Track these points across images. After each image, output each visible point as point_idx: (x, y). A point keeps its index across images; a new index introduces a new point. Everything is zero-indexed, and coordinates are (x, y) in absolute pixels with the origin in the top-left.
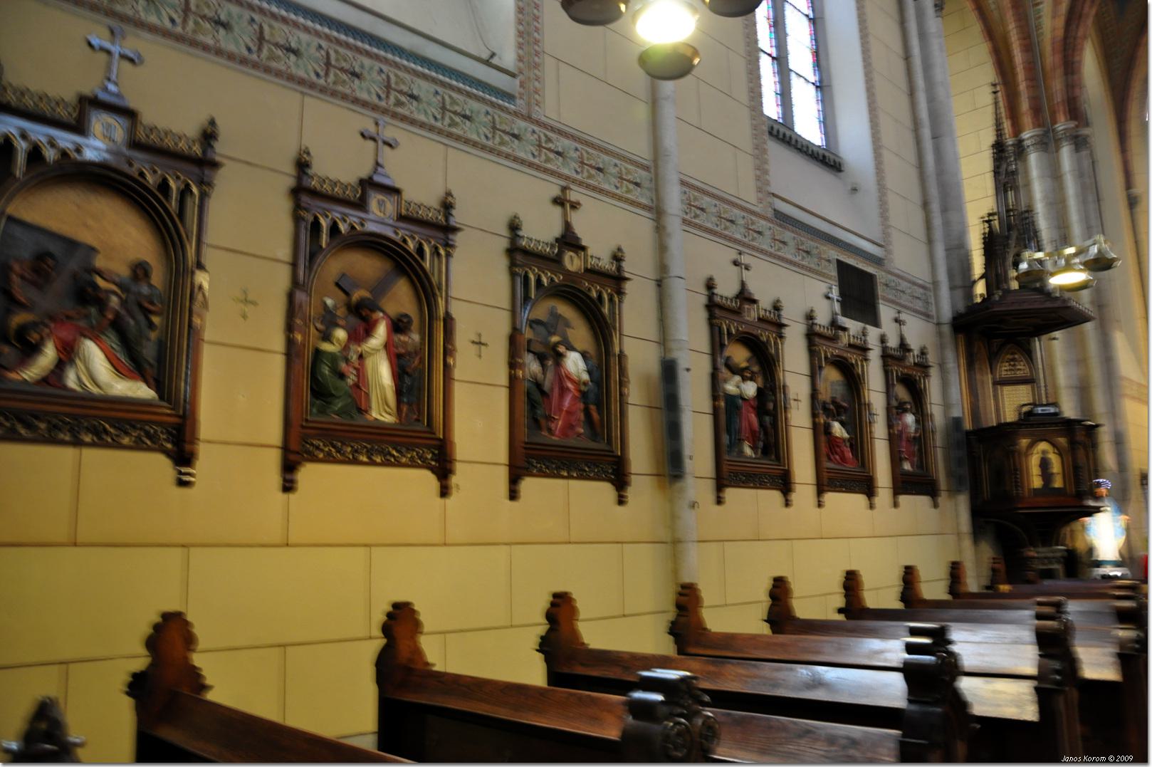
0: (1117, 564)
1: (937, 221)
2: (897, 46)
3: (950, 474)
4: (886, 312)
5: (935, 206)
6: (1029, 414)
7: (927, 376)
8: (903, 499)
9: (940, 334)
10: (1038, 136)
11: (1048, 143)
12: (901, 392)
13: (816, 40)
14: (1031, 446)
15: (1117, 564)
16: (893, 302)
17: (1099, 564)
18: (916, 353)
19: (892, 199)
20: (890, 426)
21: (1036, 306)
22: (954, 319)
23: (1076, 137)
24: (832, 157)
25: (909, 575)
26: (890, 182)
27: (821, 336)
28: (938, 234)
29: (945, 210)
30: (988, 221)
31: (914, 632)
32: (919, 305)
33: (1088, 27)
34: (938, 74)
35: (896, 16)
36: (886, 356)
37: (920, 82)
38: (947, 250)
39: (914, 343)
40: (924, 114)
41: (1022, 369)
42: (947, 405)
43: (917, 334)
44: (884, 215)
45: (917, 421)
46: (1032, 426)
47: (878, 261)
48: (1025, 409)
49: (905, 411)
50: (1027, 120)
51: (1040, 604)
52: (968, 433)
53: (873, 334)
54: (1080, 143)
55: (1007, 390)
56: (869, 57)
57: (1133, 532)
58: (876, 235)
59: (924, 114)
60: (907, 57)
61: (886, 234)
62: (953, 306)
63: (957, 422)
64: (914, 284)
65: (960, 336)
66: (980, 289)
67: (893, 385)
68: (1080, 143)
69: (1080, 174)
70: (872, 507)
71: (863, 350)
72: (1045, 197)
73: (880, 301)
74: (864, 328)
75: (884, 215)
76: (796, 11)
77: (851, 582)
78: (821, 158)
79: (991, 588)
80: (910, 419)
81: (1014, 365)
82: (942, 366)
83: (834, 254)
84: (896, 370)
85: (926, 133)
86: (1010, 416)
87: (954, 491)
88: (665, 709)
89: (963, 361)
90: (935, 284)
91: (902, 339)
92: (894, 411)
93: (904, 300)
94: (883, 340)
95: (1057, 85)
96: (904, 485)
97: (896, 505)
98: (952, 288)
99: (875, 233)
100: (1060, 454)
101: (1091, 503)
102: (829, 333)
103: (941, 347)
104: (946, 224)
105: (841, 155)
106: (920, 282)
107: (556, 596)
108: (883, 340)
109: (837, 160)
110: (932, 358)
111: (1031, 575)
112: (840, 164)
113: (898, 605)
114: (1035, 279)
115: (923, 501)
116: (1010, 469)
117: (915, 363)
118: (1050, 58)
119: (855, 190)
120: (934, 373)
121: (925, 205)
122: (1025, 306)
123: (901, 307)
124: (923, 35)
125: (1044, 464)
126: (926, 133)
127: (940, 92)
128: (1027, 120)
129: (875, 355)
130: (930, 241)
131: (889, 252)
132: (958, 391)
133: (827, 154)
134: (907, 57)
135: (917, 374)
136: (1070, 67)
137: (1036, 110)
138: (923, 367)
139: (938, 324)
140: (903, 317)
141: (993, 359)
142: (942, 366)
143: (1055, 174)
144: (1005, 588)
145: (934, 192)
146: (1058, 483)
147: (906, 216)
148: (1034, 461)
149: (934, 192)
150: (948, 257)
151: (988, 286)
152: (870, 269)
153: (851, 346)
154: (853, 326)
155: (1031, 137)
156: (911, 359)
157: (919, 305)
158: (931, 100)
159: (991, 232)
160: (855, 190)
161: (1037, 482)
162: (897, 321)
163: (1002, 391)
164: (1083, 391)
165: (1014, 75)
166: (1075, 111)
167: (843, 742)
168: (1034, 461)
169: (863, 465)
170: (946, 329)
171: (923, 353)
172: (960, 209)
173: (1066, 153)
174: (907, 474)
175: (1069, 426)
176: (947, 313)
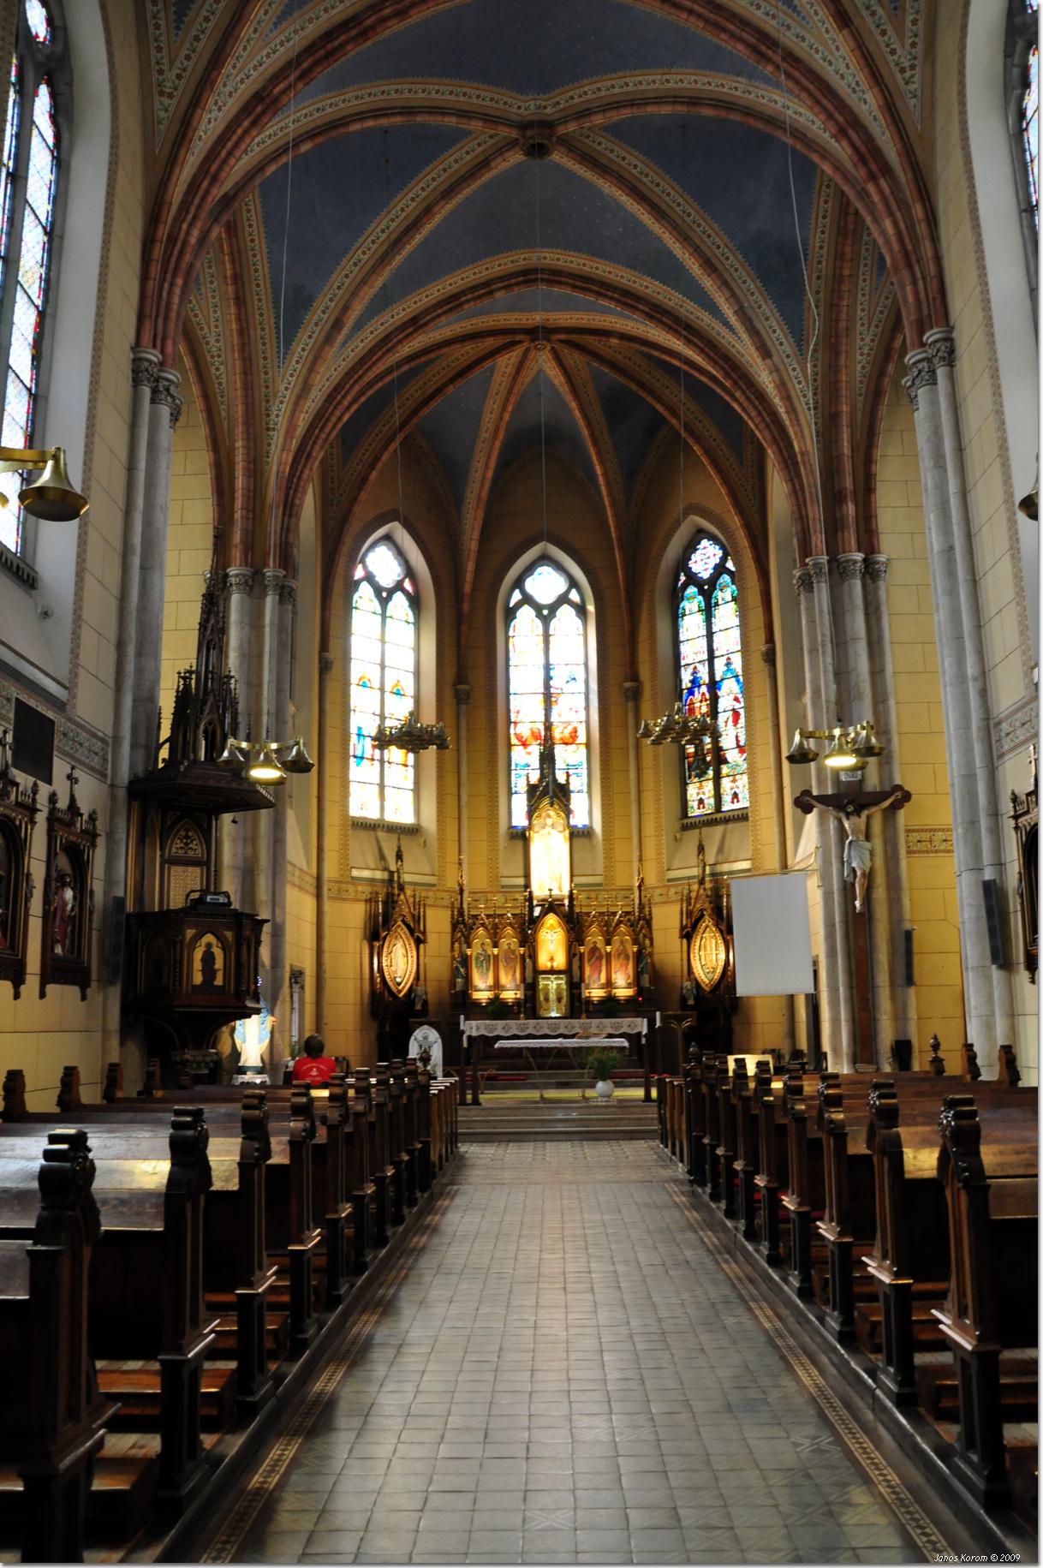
0: (260, 1071)
1: (130, 667)
2: (122, 453)
3: (103, 961)
4: (60, 767)
5: (131, 650)
6: (201, 900)
7: (94, 845)
8: (51, 989)
9: (113, 798)
10: (244, 575)
11: (254, 586)
12: (63, 862)
13: (33, 421)
14: (197, 937)
15: (260, 1071)
16: (67, 754)
17: (242, 1071)
18: (85, 817)
19: (87, 636)
20: (47, 901)
21: (223, 784)
22: (131, 782)
23: (283, 587)
24: (27, 570)
25: (70, 1077)
26: (86, 614)
27: (60, 821)
28: (129, 682)
29: (140, 654)
30: (184, 678)
31: (178, 1113)
32: (96, 762)
33: (313, 470)
34: (160, 496)
35: (127, 416)
36: (52, 819)
37: (140, 502)
38: (134, 701)
39: (85, 807)
40: (137, 540)
41: (196, 849)
42: (109, 881)
43: (89, 794)
44: (75, 652)
45: (75, 898)
46: (199, 915)
47: (60, 706)
48: (196, 896)
49: (64, 885)
50: (236, 554)
51: (178, 1113)
52: (129, 916)
53: (44, 790)
54: (286, 595)
55: (176, 871)
56: (91, 461)
57: (277, 1035)
58: (63, 672)
59: (137, 540)
60: (131, 468)
61: (74, 674)
62: (132, 766)
63: (120, 902)
64: (94, 735)
65: (136, 804)
66: (164, 753)
67: (56, 854)
68: (286, 595)
69: (280, 630)
70: (17, 996)
71: (32, 810)
72: (241, 647)
73: (55, 753)
74: (35, 785)
75: (75, 652)
76: (17, 381)
77: (15, 1080)
78: (14, 569)
79: (146, 1093)
80: (69, 894)
81: (187, 844)
82: (110, 835)
83: (15, 692)
84: (62, 836)
85: (136, 561)
86: (177, 901)
87: (106, 983)
88: (72, 1154)
89: (133, 832)
90: (117, 738)
91: (73, 799)
92: (54, 882)
93: (81, 754)
94: (53, 798)
95: (273, 526)
96: (53, 972)
97: (42, 995)
98: (133, 746)
99: (63, 672)
100: (224, 949)
101: (250, 1004)
102: (67, 818)
103: (113, 814)
104: (140, 670)
105: (37, 569)
106: (100, 734)
107: (66, 1069)
108: (53, 798)
109: (32, 574)
110: (100, 826)
111: (185, 1080)
112: (34, 580)
113: (57, 1110)
114: (238, 769)
115: (74, 991)
116: (171, 960)
117: (17, 802)
118: (273, 493)
119: (46, 614)
120: (101, 842)
121: (120, 645)
122: (211, 783)
123: (76, 762)
124: (152, 446)
125: (208, 958)
126: (136, 561)
127: (159, 516)
128: (236, 554)
129: (41, 818)
130: (118, 689)
131: (74, 696)
132: (124, 867)
133: (22, 565)
134: (131, 468)
135: (84, 843)
136: (290, 508)
137: (249, 546)
138: (92, 836)
139: (113, 786)
140: (77, 773)
141: (165, 835)
142: (110, 835)
143: (254, 622)
144: (159, 1094)
145: (132, 631)
146: (219, 981)
147: (97, 656)
148: (198, 954)
149: (132, 631)
150: (134, 708)
151: (172, 751)
152: (50, 715)
153: (18, 804)
154: (23, 779)
155: (237, 575)
156: (81, 824)
157: (96, 762)
158: (148, 523)
159: (187, 687)
160: (46, 614)
161: (198, 978)
162: (69, 777)
163: (169, 869)
164: (248, 874)
165: (232, 499)
166: (286, 560)
167: (115, 1202)
168: (198, 954)
169: (13, 946)
170: (122, 794)
171: (93, 818)
172: (156, 656)
173: (270, 601)
174: (57, 958)
175: (237, 916)
176: (124, 775)
